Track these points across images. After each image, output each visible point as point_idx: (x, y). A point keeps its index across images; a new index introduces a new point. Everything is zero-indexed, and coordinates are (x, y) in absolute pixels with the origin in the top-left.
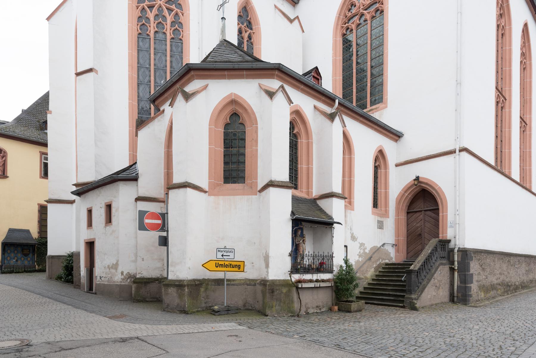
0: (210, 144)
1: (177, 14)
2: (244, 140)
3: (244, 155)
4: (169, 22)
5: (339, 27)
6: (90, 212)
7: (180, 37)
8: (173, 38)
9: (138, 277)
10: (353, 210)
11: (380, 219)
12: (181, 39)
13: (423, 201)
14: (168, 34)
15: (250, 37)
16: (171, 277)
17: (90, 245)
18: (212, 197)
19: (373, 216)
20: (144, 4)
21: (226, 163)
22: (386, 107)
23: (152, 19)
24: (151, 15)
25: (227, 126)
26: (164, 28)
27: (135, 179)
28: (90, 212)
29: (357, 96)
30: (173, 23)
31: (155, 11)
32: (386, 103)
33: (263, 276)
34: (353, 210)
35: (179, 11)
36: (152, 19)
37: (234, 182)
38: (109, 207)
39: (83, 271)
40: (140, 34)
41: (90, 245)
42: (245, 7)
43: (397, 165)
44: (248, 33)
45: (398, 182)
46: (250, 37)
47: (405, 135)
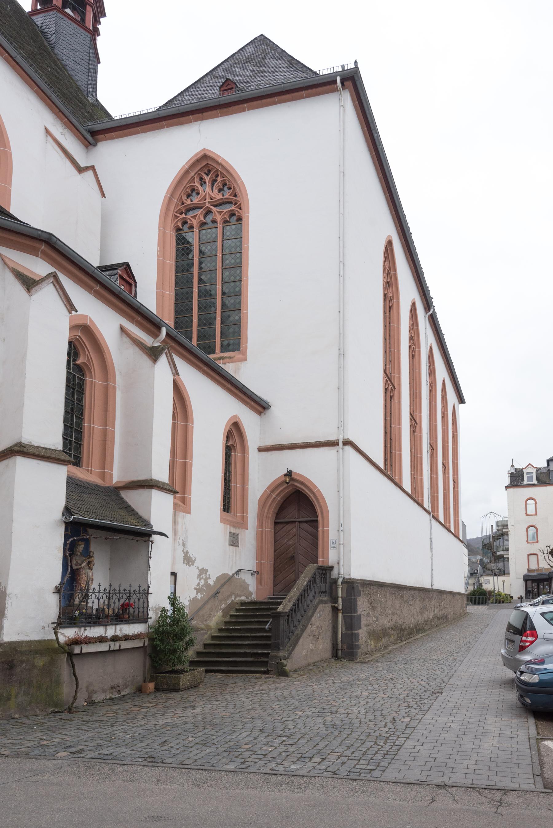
5: (171, 214)
10: (189, 513)
11: (233, 530)
32: (245, 354)
43: (260, 450)
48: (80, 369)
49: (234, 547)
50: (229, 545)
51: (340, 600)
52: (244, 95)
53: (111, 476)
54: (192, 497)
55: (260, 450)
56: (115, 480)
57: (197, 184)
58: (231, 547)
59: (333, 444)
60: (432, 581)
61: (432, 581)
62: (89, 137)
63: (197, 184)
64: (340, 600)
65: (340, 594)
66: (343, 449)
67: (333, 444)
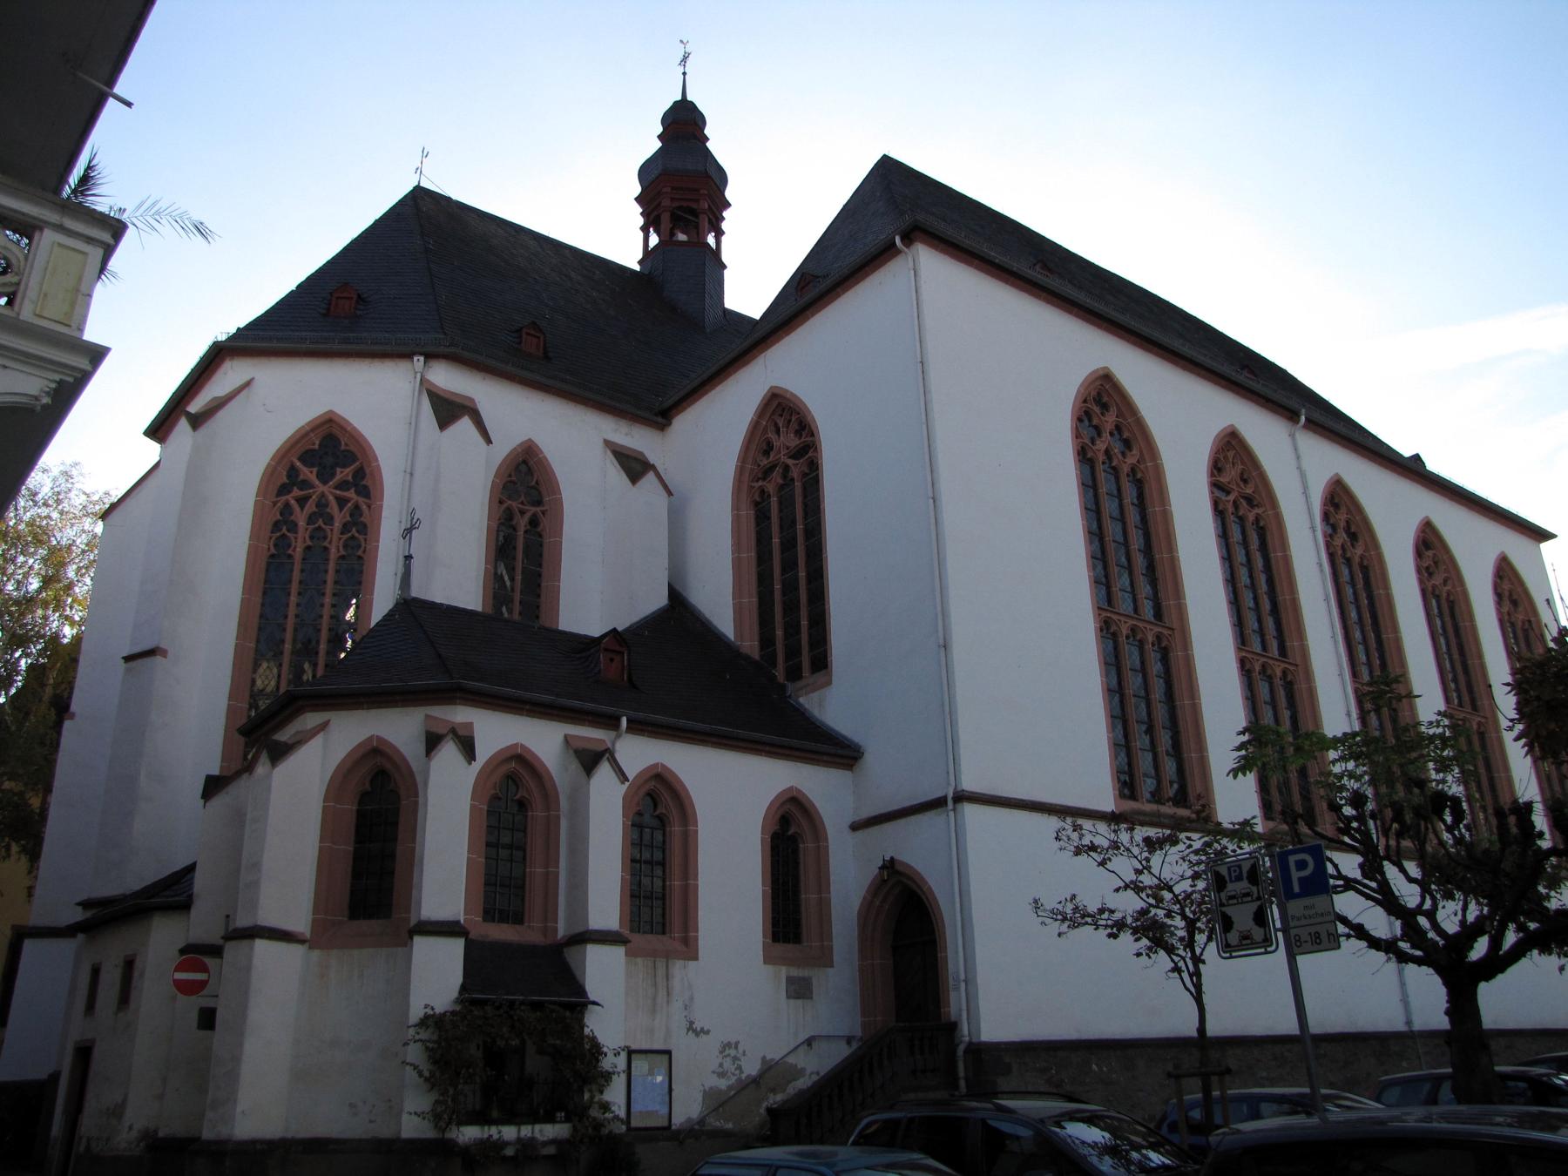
0: (322, 839)
1: (357, 507)
2: (396, 824)
3: (393, 856)
4: (337, 525)
5: (745, 488)
6: (96, 972)
7: (360, 553)
8: (343, 557)
9: (161, 1134)
10: (696, 958)
11: (795, 972)
12: (360, 558)
13: (909, 925)
14: (333, 550)
15: (534, 522)
16: (207, 1134)
17: (84, 1053)
18: (316, 954)
19: (770, 968)
20: (289, 497)
21: (356, 875)
22: (829, 683)
23: (302, 523)
24: (301, 518)
25: (364, 798)
26: (325, 538)
27: (185, 906)
28: (96, 972)
29: (810, 635)
30: (346, 528)
31: (310, 507)
32: (830, 675)
33: (385, 1132)
34: (696, 958)
35: (361, 500)
36: (302, 523)
37: (370, 917)
38: (129, 964)
39: (57, 1128)
40: (272, 556)
41: (84, 1053)
42: (525, 462)
43: (856, 827)
44: (527, 517)
45: (848, 874)
46: (534, 522)
47: (866, 755)
48: (1262, 528)
49: (800, 1002)
50: (788, 997)
51: (962, 1083)
52: (829, 282)
53: (556, 930)
54: (701, 934)
55: (856, 827)
56: (561, 933)
57: (772, 435)
58: (792, 1001)
59: (938, 804)
60: (1405, 1001)
61: (1405, 1001)
62: (660, 419)
63: (772, 435)
64: (962, 1083)
65: (961, 1073)
66: (954, 810)
67: (938, 804)
